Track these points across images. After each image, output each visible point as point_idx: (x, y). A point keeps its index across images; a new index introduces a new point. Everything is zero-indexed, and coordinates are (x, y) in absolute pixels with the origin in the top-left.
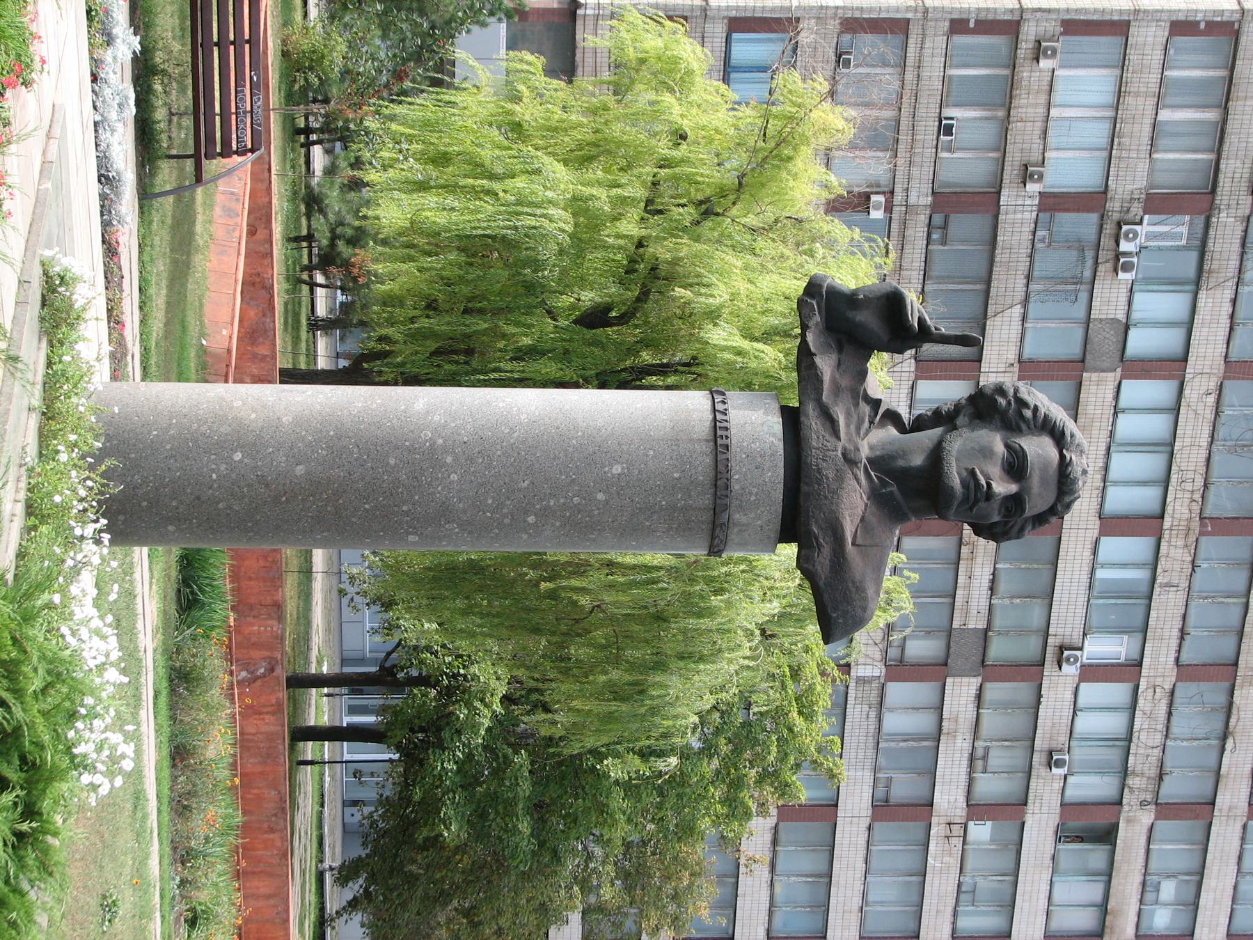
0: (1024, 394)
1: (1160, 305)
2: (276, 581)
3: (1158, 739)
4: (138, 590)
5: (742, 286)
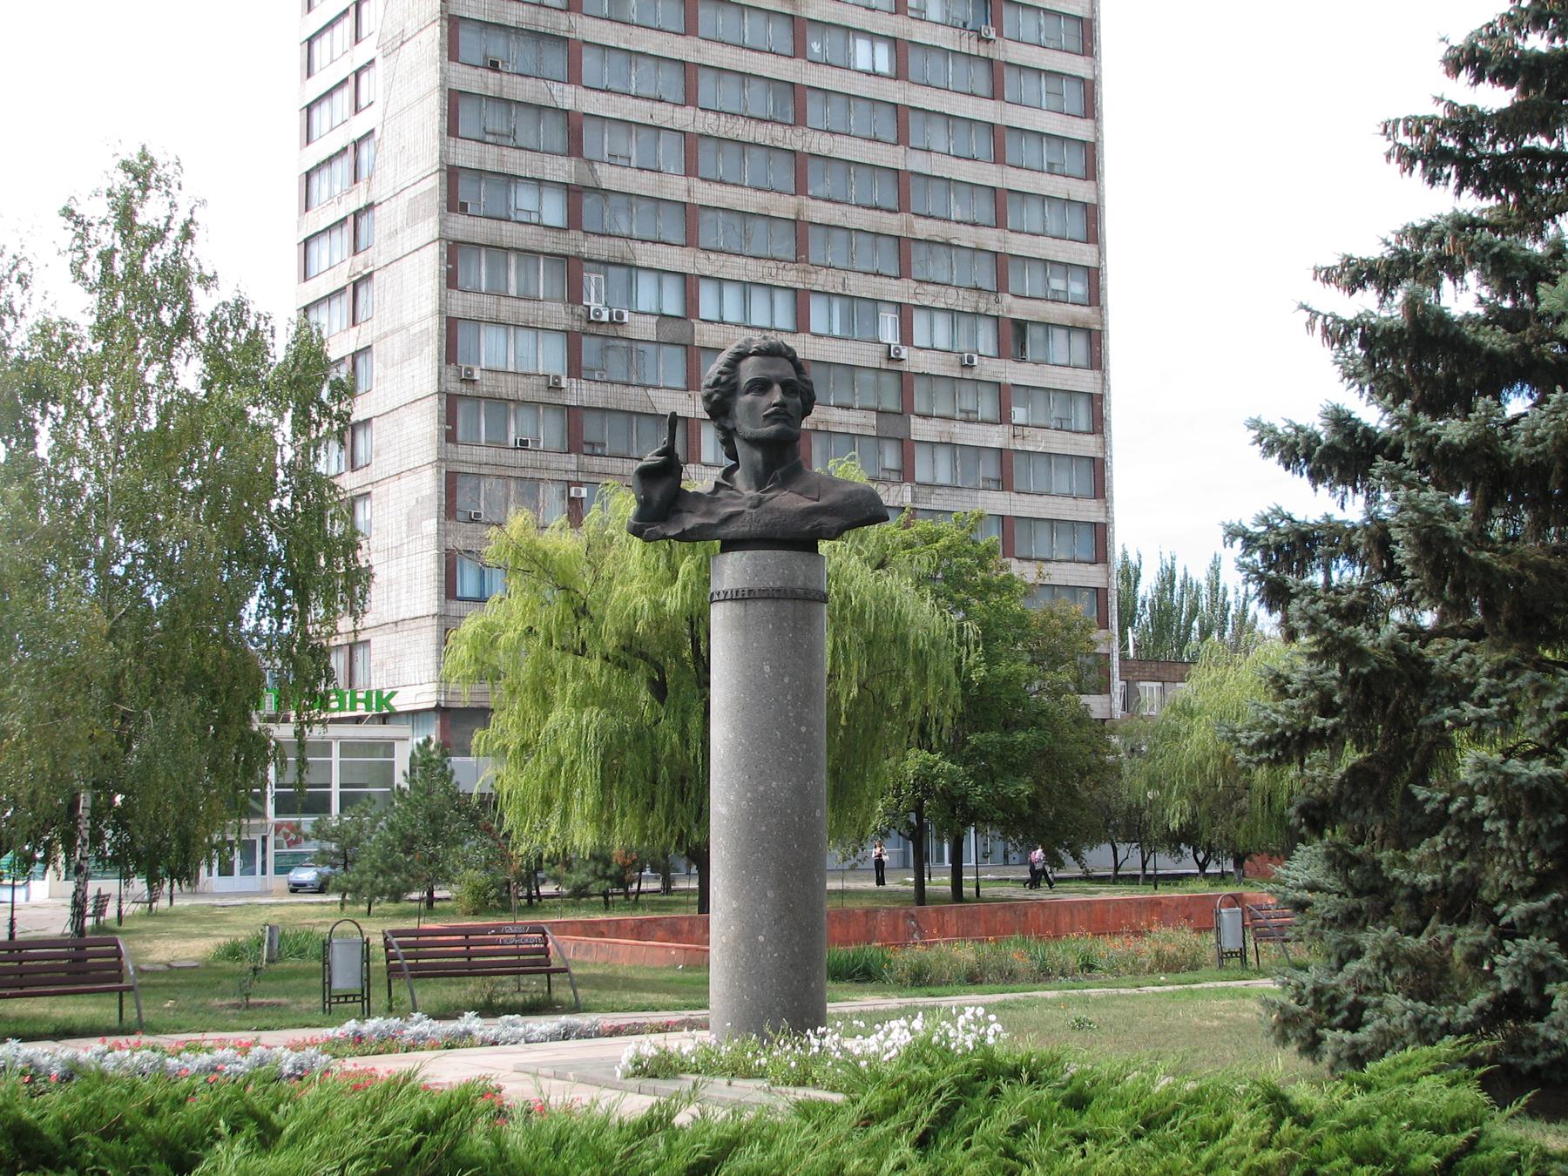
0: (711, 381)
1: (646, 293)
2: (850, 915)
3: (952, 291)
4: (857, 1009)
5: (636, 585)
